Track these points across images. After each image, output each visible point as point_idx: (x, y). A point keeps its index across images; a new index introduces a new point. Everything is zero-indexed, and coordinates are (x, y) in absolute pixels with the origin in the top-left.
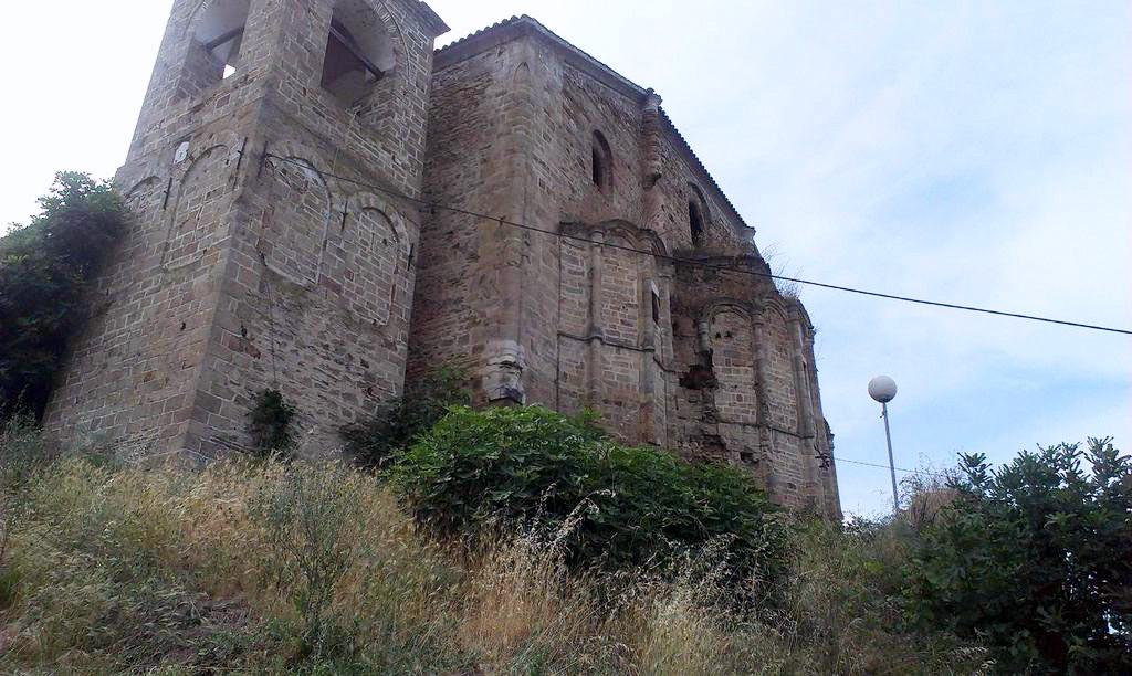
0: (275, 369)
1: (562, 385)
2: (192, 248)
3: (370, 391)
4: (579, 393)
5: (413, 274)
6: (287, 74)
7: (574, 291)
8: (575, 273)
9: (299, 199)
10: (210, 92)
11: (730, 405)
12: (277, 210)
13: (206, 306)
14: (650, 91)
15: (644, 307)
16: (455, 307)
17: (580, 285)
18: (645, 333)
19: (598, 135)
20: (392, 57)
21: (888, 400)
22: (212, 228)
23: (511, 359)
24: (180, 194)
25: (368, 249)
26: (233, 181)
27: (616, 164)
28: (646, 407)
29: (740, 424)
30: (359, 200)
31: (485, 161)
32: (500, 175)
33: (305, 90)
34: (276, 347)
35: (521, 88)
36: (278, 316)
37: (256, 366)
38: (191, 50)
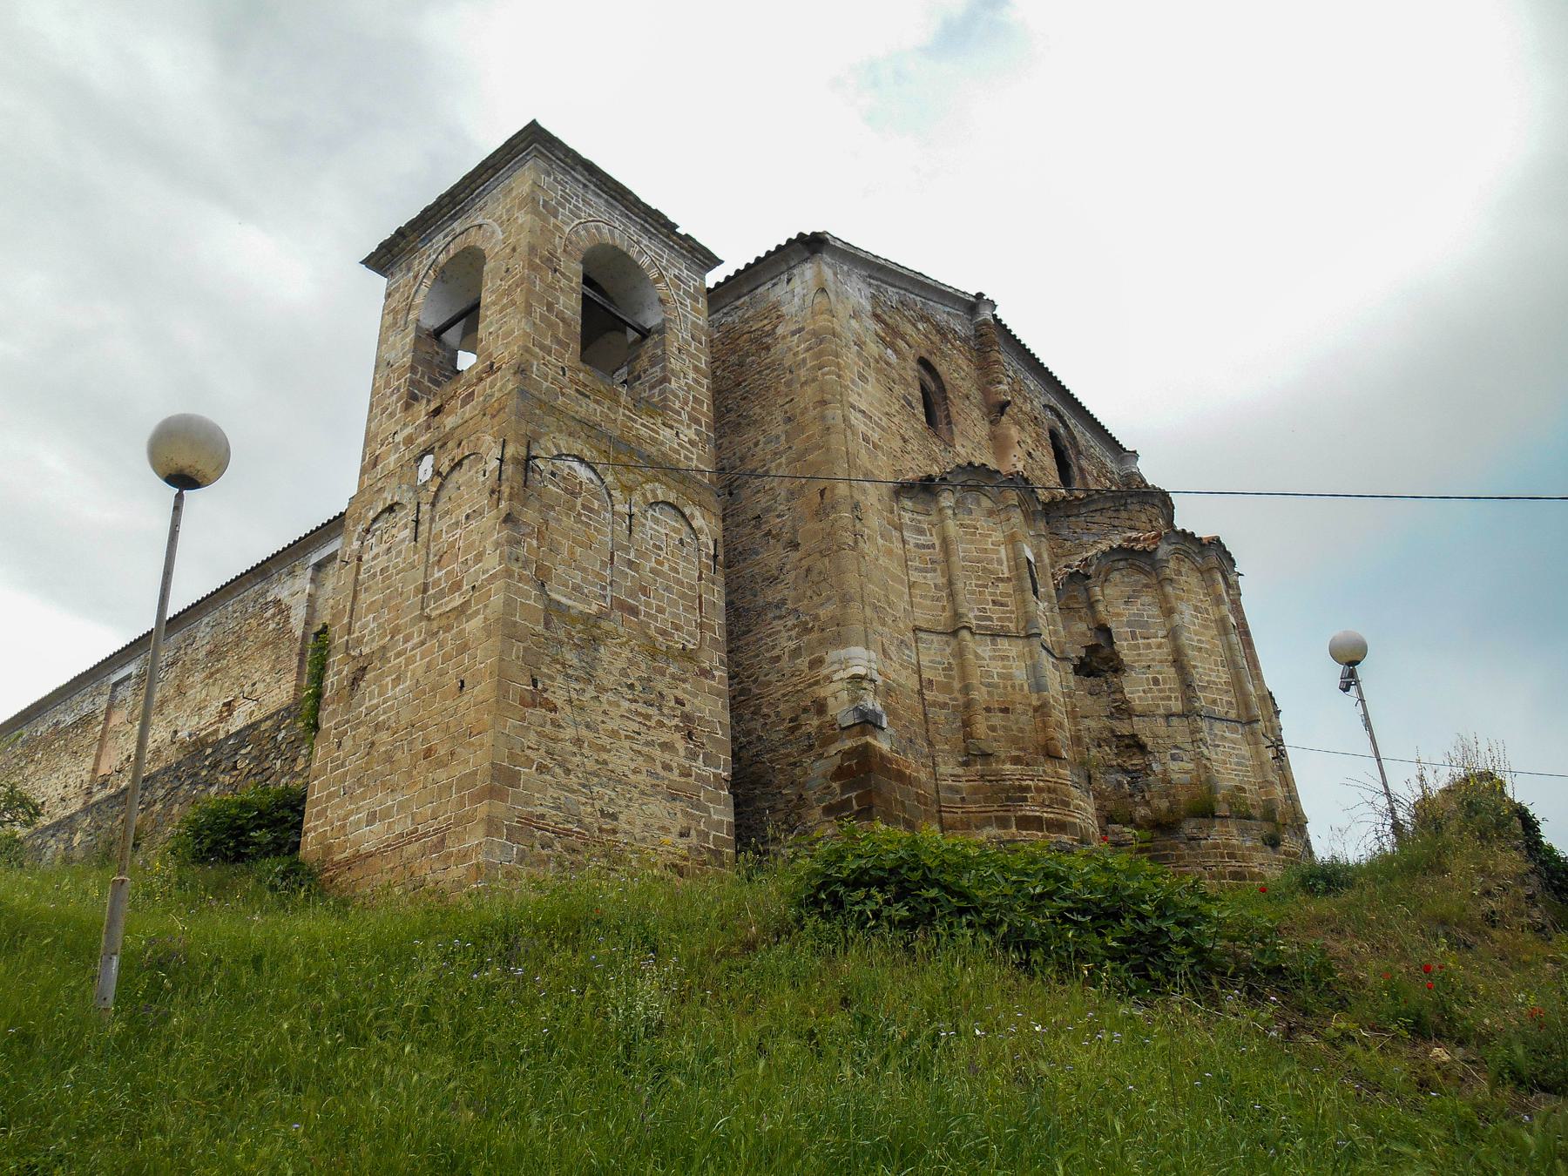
0: (576, 724)
1: (929, 695)
2: (457, 586)
3: (690, 735)
4: (951, 703)
5: (721, 579)
6: (541, 353)
9: (574, 506)
10: (449, 388)
11: (1144, 691)
12: (552, 524)
13: (484, 658)
14: (980, 296)
15: (1019, 578)
16: (777, 613)
17: (933, 562)
19: (924, 363)
21: (1358, 663)
22: (479, 558)
23: (861, 671)
24: (432, 520)
25: (663, 554)
26: (495, 496)
28: (1042, 710)
29: (1160, 716)
30: (644, 495)
31: (789, 419)
32: (813, 435)
33: (563, 369)
34: (574, 695)
35: (823, 321)
36: (571, 657)
37: (554, 723)
38: (418, 339)
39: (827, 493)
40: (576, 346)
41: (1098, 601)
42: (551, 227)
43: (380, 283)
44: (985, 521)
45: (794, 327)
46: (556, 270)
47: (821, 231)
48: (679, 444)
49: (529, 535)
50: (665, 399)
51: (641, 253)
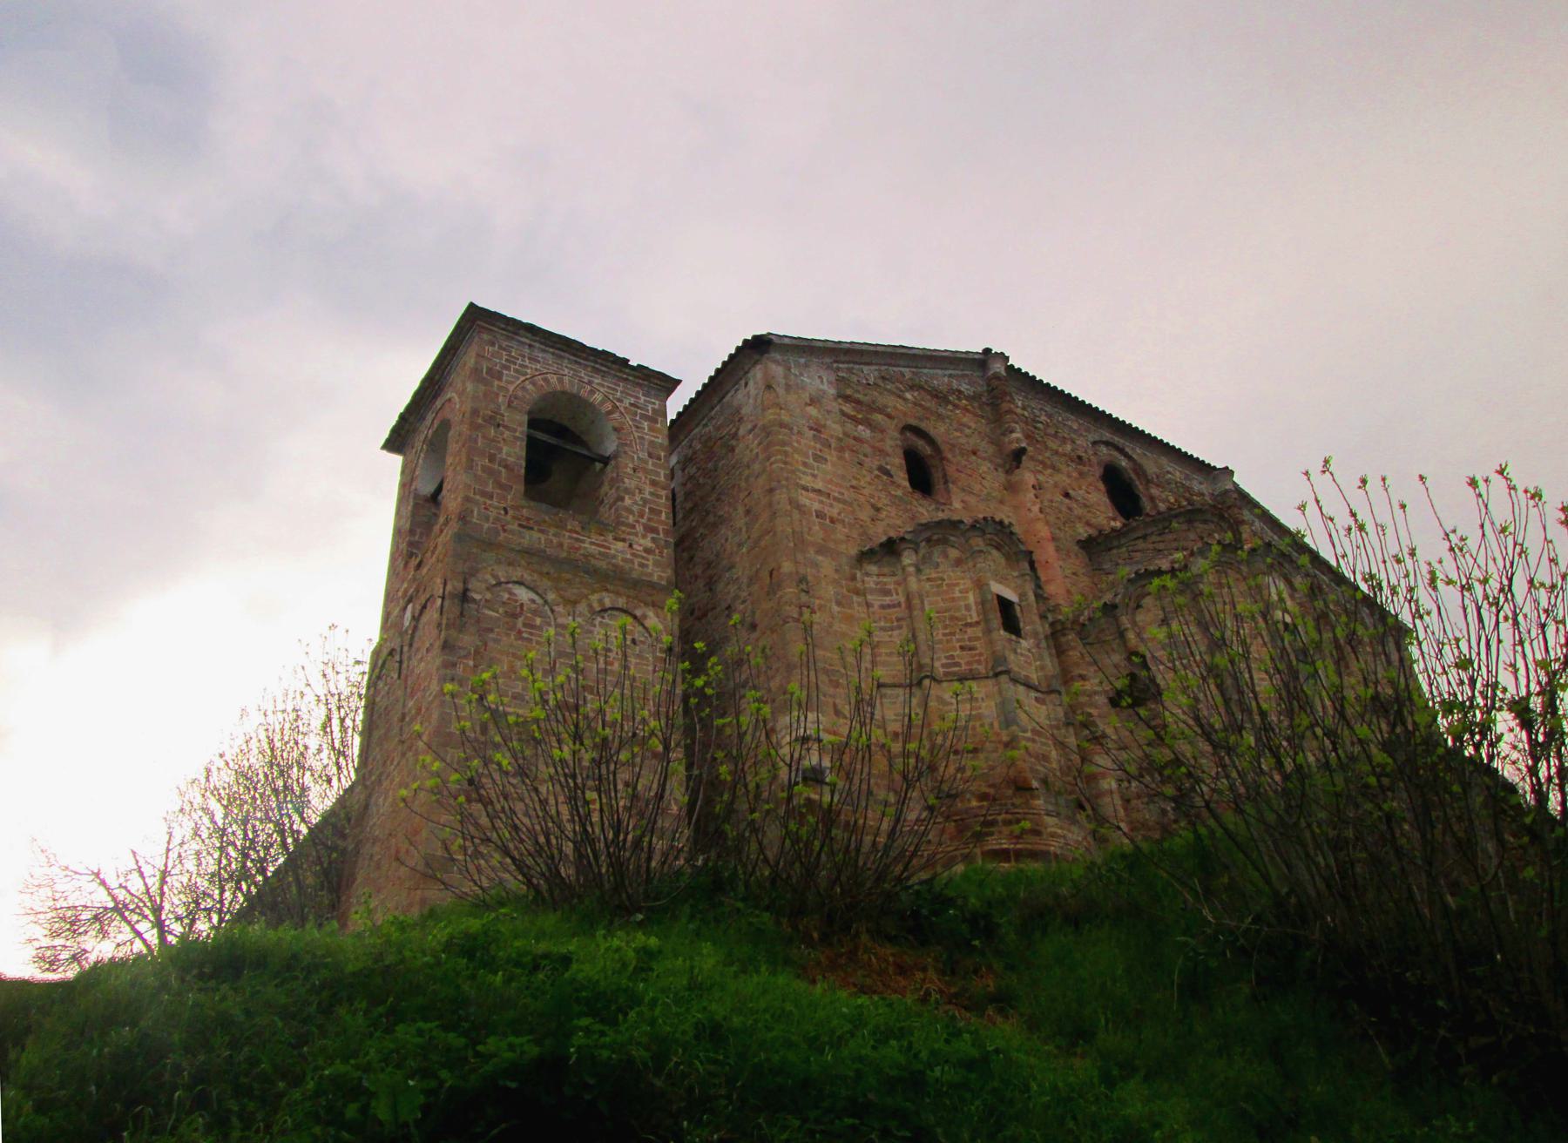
6: (482, 500)
7: (892, 629)
8: (889, 606)
9: (515, 624)
12: (491, 644)
14: (987, 351)
15: (987, 621)
18: (994, 652)
20: (614, 436)
27: (949, 456)
30: (590, 606)
38: (416, 506)
39: (775, 573)
40: (519, 487)
41: (1126, 629)
42: (495, 389)
43: (397, 460)
44: (953, 571)
45: (750, 426)
46: (499, 425)
47: (764, 333)
48: (633, 554)
49: (465, 657)
50: (618, 516)
51: (592, 392)
